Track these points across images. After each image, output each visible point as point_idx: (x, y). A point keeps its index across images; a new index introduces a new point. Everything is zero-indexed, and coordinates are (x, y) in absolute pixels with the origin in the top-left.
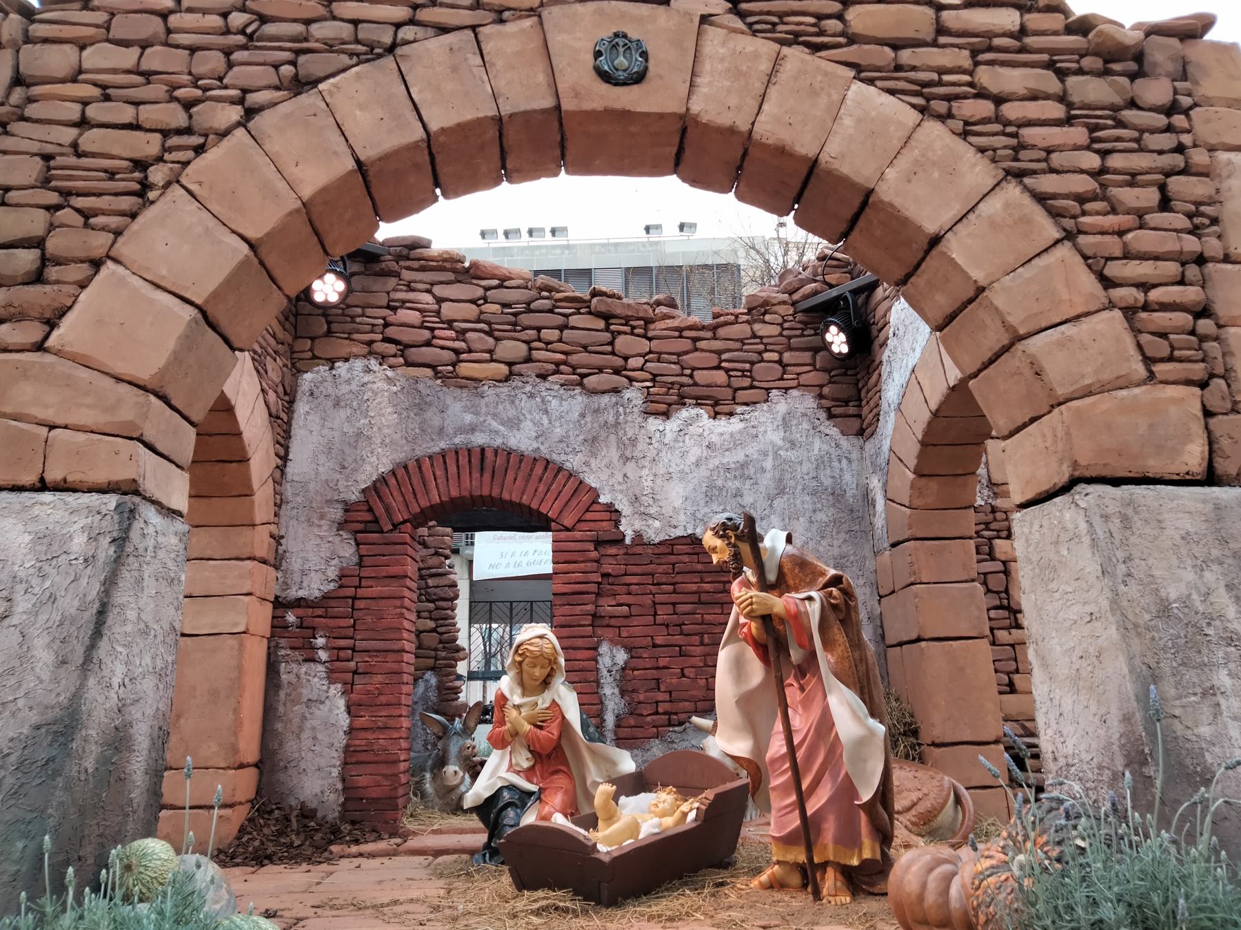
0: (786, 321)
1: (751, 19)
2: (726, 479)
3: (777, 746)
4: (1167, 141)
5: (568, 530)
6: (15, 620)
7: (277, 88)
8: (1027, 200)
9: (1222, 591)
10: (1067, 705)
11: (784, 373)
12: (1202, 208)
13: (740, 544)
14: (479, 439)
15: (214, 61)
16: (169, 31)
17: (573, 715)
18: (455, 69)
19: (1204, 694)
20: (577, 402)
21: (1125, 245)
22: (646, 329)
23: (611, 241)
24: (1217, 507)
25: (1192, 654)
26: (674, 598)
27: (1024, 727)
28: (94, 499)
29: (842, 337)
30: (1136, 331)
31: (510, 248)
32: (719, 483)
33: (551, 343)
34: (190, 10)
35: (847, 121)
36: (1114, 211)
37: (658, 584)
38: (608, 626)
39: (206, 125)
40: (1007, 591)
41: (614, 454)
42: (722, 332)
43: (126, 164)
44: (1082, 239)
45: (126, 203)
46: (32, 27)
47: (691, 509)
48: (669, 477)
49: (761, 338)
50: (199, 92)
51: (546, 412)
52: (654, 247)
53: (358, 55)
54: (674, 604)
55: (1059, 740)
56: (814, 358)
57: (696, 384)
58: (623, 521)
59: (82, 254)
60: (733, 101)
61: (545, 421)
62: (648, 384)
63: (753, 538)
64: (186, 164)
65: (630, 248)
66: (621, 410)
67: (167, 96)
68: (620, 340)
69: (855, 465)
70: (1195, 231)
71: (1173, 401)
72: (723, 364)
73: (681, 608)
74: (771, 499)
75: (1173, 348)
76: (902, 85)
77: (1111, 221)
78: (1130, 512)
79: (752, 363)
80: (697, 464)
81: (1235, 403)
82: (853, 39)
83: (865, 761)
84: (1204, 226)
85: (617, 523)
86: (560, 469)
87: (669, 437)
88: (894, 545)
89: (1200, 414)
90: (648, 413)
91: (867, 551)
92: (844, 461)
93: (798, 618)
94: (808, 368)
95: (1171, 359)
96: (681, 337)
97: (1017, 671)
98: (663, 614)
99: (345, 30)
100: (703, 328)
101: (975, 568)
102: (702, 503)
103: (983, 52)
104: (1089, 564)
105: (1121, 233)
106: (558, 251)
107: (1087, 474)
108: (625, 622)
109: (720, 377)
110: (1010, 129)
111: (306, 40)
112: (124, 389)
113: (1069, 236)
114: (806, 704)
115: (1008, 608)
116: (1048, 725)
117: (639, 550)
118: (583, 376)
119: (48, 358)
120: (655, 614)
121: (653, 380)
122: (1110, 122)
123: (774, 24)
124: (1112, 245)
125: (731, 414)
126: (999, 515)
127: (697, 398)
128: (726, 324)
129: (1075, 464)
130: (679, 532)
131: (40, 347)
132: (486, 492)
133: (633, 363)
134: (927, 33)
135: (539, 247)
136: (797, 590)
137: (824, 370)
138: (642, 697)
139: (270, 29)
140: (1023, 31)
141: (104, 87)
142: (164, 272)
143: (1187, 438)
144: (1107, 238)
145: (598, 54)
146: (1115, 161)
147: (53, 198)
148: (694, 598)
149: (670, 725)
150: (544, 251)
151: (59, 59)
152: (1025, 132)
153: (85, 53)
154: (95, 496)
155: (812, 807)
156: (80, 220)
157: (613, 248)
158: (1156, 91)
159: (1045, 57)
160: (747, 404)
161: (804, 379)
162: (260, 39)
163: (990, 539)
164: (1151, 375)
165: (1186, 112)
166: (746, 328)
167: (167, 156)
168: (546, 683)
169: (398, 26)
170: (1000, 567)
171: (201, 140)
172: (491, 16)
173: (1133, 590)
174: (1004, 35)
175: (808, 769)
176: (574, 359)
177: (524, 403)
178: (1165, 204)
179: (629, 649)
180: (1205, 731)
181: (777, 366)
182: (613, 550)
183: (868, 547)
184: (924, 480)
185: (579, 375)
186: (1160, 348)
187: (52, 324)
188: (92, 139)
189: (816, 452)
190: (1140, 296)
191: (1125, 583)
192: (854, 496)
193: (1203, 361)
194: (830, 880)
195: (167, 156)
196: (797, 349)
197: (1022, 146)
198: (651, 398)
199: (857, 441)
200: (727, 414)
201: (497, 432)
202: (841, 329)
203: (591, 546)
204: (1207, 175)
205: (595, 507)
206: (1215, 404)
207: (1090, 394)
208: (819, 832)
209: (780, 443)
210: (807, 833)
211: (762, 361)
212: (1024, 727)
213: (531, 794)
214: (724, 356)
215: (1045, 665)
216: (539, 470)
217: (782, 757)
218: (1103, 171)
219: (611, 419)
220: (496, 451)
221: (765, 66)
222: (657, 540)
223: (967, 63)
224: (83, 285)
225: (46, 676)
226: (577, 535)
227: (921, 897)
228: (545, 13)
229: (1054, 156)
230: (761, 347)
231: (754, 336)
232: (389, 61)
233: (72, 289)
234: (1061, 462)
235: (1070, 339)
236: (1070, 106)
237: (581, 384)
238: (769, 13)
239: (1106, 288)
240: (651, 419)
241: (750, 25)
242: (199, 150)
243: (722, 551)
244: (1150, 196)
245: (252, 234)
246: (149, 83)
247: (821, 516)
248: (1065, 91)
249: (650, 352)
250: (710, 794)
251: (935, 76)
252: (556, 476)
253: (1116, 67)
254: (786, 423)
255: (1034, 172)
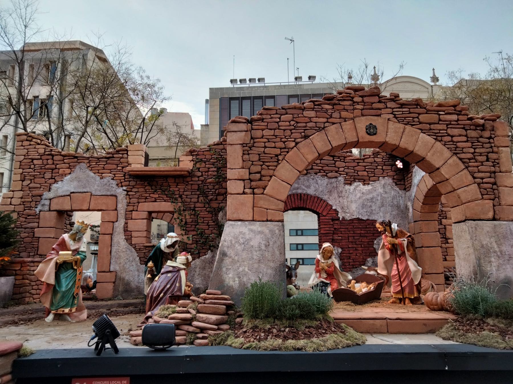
0: (384, 157)
1: (398, 119)
2: (367, 202)
3: (394, 272)
4: (488, 145)
5: (324, 216)
6: (271, 246)
7: (301, 138)
8: (458, 160)
9: (494, 242)
10: (463, 263)
11: (383, 172)
12: (496, 161)
13: (386, 227)
14: (300, 191)
15: (288, 133)
16: (279, 126)
17: (337, 265)
18: (337, 133)
19: (489, 262)
20: (326, 180)
21: (478, 169)
22: (344, 160)
23: (282, 84)
24: (495, 226)
25: (487, 255)
26: (354, 235)
27: (449, 270)
28: (277, 223)
29: (401, 164)
30: (480, 188)
31: (243, 87)
32: (366, 203)
33: (318, 164)
34: (283, 121)
35: (420, 142)
36: (476, 162)
37: (350, 231)
38: (336, 242)
39: (289, 147)
40: (445, 233)
41: (336, 195)
42: (366, 160)
43: (274, 156)
44: (469, 168)
45: (275, 164)
46: (253, 126)
47: (358, 211)
48: (352, 202)
49: (377, 162)
50: (286, 140)
51: (317, 184)
52: (300, 87)
53: (317, 130)
54: (354, 237)
55: (460, 271)
56: (392, 168)
57: (358, 175)
58: (339, 214)
59: (268, 175)
60: (395, 138)
61: (317, 186)
62: (345, 175)
63: (389, 224)
64: (285, 155)
65: (290, 87)
66: (338, 183)
67: (280, 141)
68: (337, 163)
69: (403, 198)
70: (494, 166)
71: (487, 203)
72: (366, 170)
73: (356, 238)
74: (380, 208)
75: (487, 192)
76: (431, 134)
77: (476, 164)
78: (477, 227)
79: (374, 169)
80: (359, 198)
81: (500, 203)
82: (421, 123)
83: (417, 275)
84: (496, 165)
85: (337, 214)
86: (322, 200)
87: (351, 190)
88: (415, 222)
89: (492, 206)
90: (345, 184)
91: (406, 222)
92: (400, 197)
93: (401, 245)
94: (390, 171)
95: (487, 194)
96: (354, 162)
97: (447, 255)
98: (351, 239)
99: (314, 124)
100: (360, 159)
101: (438, 227)
102: (361, 209)
103: (449, 125)
104: (468, 237)
105: (478, 167)
106: (262, 89)
107: (468, 219)
108: (341, 241)
109: (365, 173)
110: (455, 143)
111: (306, 127)
112: (279, 202)
113: (467, 168)
114: (401, 263)
115: (445, 238)
116: (458, 268)
117: (344, 222)
118: (327, 173)
119: (265, 196)
120: (349, 239)
121: (346, 174)
122: (476, 141)
123: (403, 120)
124: (476, 169)
125: (369, 184)
126: (444, 213)
127: (359, 179)
128: (367, 158)
129: (466, 217)
130: (355, 217)
131: (263, 194)
132: (302, 206)
133: (341, 169)
134: (437, 121)
135: (254, 87)
136: (400, 238)
137: (394, 171)
138: (346, 261)
139: (299, 125)
140: (458, 120)
141: (268, 139)
142: (284, 178)
143: (489, 211)
144: (475, 168)
145: (367, 129)
146: (477, 150)
147: (262, 163)
148: (359, 235)
149: (353, 268)
150: (256, 88)
151: (259, 133)
152: (458, 144)
153: (264, 132)
154: (277, 223)
155: (403, 285)
156: (267, 168)
157: (283, 87)
158: (487, 134)
159: (463, 126)
160: (373, 181)
161: (389, 174)
162: (297, 127)
163: (441, 219)
164: (483, 198)
165: (493, 139)
166: (373, 159)
167: (282, 154)
168: (330, 257)
169: (324, 123)
170: (443, 227)
171: (288, 150)
172: (344, 120)
173: (477, 242)
174: (454, 121)
175: (402, 278)
176: (324, 168)
177: (311, 181)
178: (488, 160)
179: (342, 248)
180: (489, 269)
181: (381, 170)
182: (337, 222)
183: (407, 221)
184: (424, 206)
185: (326, 173)
186: (485, 192)
187: (264, 189)
188: (267, 150)
189: (392, 195)
190: (481, 181)
191: (475, 241)
192: (403, 207)
193: (494, 195)
194: (407, 301)
195: (282, 154)
196: (387, 165)
197: (457, 147)
198: (346, 179)
199: (404, 192)
200: (367, 184)
201: (304, 189)
202: (401, 162)
203: (331, 221)
204: (497, 153)
205: (332, 210)
206: (496, 204)
207: (470, 202)
208: (404, 291)
209: (382, 192)
210: (402, 291)
211: (377, 169)
212: (449, 270)
213: (328, 284)
214: (366, 167)
215: (458, 256)
216: (316, 200)
217: (396, 275)
218: (475, 152)
219: (335, 186)
220: (304, 195)
221: (402, 130)
222: (349, 219)
223: (446, 128)
224: (269, 181)
225: (279, 256)
226: (327, 217)
227: (432, 300)
228: (355, 119)
229: (464, 149)
230: (377, 165)
231: (375, 161)
232: (323, 131)
233: (267, 182)
234: (463, 216)
235: (466, 190)
236: (468, 138)
237: (326, 176)
238: (402, 117)
239: (474, 179)
240: (346, 186)
241: (398, 120)
242: (288, 152)
243: (381, 228)
244: (484, 158)
245: (300, 170)
246: (276, 138)
247: (394, 213)
248: (467, 134)
249: (346, 166)
250: (377, 283)
251: (438, 131)
252: (320, 202)
253: (478, 128)
254: (384, 187)
255: (459, 153)
